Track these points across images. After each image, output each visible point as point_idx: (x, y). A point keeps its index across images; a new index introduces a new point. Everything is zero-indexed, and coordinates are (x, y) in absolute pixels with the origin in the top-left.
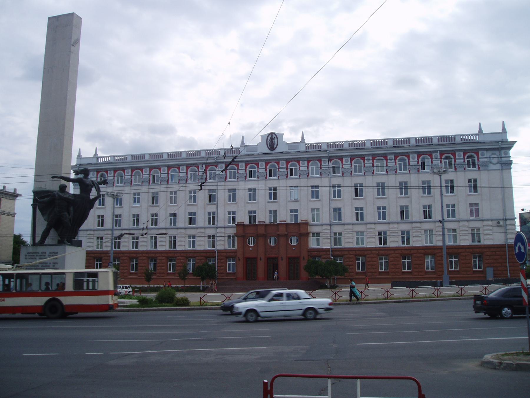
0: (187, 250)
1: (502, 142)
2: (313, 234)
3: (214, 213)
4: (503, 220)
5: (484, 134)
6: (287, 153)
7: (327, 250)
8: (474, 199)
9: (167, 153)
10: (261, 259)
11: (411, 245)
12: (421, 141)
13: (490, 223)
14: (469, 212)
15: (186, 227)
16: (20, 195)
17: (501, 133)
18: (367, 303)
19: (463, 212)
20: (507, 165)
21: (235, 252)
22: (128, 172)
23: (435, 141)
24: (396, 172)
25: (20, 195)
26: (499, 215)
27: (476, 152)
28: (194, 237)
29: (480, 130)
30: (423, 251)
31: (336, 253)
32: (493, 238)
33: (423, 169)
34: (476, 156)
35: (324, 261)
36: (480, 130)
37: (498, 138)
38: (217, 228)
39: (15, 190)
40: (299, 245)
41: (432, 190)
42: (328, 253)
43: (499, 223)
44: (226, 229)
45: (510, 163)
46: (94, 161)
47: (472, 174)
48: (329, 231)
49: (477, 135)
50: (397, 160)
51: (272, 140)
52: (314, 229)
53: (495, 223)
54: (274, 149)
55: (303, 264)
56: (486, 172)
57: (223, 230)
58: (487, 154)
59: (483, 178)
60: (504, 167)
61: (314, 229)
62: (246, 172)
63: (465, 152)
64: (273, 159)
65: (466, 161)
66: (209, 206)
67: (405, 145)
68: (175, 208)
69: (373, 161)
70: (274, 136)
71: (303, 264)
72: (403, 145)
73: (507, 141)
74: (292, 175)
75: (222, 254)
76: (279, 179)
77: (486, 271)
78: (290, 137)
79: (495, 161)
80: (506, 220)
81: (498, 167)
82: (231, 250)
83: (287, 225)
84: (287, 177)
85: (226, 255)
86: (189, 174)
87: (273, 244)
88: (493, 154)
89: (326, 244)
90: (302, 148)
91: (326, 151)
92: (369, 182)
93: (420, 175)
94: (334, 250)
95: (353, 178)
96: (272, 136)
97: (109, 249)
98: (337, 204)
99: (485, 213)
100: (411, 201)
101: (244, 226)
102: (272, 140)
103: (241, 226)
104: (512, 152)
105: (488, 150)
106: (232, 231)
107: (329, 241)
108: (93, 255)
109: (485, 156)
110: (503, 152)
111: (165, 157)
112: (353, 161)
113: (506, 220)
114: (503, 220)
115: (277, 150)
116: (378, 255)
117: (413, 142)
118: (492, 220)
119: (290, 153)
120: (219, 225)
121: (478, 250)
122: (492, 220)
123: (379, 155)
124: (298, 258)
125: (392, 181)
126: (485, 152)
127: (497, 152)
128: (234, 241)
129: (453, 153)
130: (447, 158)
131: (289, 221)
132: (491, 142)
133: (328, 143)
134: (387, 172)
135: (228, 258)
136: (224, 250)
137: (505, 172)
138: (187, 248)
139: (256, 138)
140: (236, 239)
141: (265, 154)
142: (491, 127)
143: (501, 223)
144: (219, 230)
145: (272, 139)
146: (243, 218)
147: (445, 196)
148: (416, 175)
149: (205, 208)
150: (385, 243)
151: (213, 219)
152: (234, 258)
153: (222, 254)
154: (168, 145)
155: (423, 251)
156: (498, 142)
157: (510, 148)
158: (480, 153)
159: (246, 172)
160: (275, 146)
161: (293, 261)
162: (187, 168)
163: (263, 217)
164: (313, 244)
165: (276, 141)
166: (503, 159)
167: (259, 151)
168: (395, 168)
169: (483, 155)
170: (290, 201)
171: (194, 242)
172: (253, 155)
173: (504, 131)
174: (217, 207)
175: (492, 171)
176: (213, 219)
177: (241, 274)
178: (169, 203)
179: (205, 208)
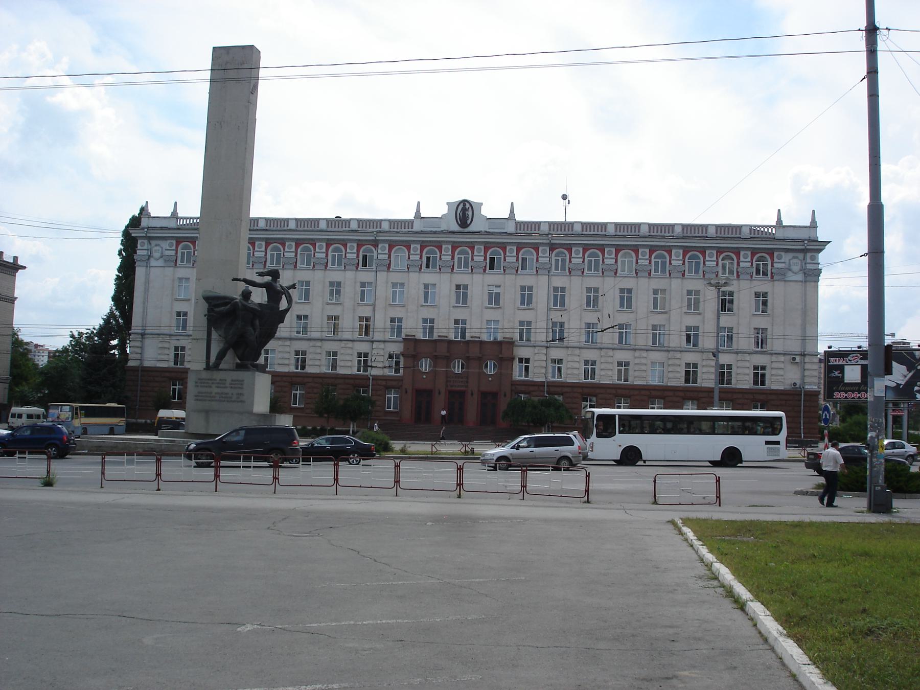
0: (325, 374)
1: (810, 240)
2: (521, 360)
3: (367, 319)
4: (801, 355)
5: (784, 227)
6: (487, 233)
7: (540, 385)
8: (761, 322)
9: (296, 220)
10: (439, 393)
11: (698, 385)
12: (690, 230)
13: (782, 358)
14: (685, 338)
15: (355, 338)
16: (24, 268)
17: (810, 227)
18: (410, 458)
19: (745, 342)
20: (812, 275)
21: (400, 380)
22: (321, 248)
23: (678, 230)
24: (650, 274)
25: (24, 268)
26: (795, 347)
27: (771, 252)
28: (335, 354)
29: (779, 221)
30: (681, 394)
31: (552, 389)
32: (782, 377)
33: (492, 267)
34: (769, 260)
35: (536, 399)
36: (779, 221)
37: (803, 235)
38: (372, 342)
39: (16, 258)
40: (499, 376)
41: (701, 304)
42: (541, 388)
43: (794, 359)
44: (387, 344)
45: (818, 272)
46: (172, 224)
47: (762, 285)
48: (807, 366)
49: (774, 227)
50: (299, 250)
51: (464, 211)
52: (522, 352)
53: (789, 358)
54: (467, 226)
55: (503, 404)
56: (783, 283)
57: (382, 345)
58: (786, 257)
59: (777, 292)
60: (808, 278)
61: (522, 352)
62: (421, 258)
63: (754, 252)
64: (464, 238)
65: (754, 266)
66: (361, 308)
67: (667, 234)
68: (306, 307)
69: (616, 255)
70: (468, 206)
71: (503, 404)
72: (663, 234)
73: (816, 241)
74: (492, 267)
75: (379, 382)
76: (345, 270)
77: (9, 398)
78: (493, 208)
79: (796, 268)
80: (805, 355)
81: (800, 277)
82: (329, 374)
83: (482, 343)
84: (485, 270)
85: (385, 384)
86: (330, 254)
87: (458, 370)
88: (794, 258)
89: (538, 374)
90: (511, 228)
91: (547, 235)
92: (610, 287)
93: (486, 276)
94: (551, 385)
95: (390, 274)
96: (465, 205)
97: (711, 384)
98: (658, 319)
99: (774, 345)
100: (669, 320)
101: (417, 342)
102: (464, 211)
103: (411, 342)
104: (822, 257)
105: (787, 251)
106: (397, 348)
107: (544, 371)
108: (167, 374)
109: (782, 260)
110: (809, 255)
111: (292, 226)
112: (554, 253)
113: (805, 355)
114: (801, 355)
115: (472, 228)
116: (616, 396)
117: (644, 230)
118: (784, 354)
119: (492, 234)
120: (376, 337)
121: (761, 397)
122: (784, 354)
123: (431, 243)
124: (495, 395)
125: (643, 289)
126: (783, 254)
127: (801, 256)
128: (397, 363)
129: (737, 252)
130: (274, 249)
131: (452, 337)
132: (793, 240)
133: (751, 226)
134: (637, 273)
135: (388, 388)
136: (383, 376)
137: (810, 285)
138: (325, 369)
139: (436, 208)
140: (402, 360)
141: (453, 232)
142: (796, 217)
143: (798, 359)
144: (375, 345)
145: (464, 210)
146: (414, 327)
147: (296, 303)
148: (680, 280)
149: (354, 310)
150: (763, 383)
151: (366, 327)
152: (398, 388)
153: (379, 382)
154: (582, 212)
155: (681, 394)
156: (803, 241)
157: (820, 251)
158: (776, 254)
159: (421, 258)
160: (469, 222)
161: (488, 398)
162: (267, 245)
163: (445, 329)
164: (517, 374)
165: (470, 213)
166: (809, 266)
167: (444, 227)
168: (615, 268)
169: (780, 257)
170: (480, 307)
171: (335, 361)
172: (435, 233)
173: (814, 225)
174: (374, 310)
175: (791, 283)
176: (366, 327)
177: (407, 413)
178: (685, 309)
179: (354, 310)
